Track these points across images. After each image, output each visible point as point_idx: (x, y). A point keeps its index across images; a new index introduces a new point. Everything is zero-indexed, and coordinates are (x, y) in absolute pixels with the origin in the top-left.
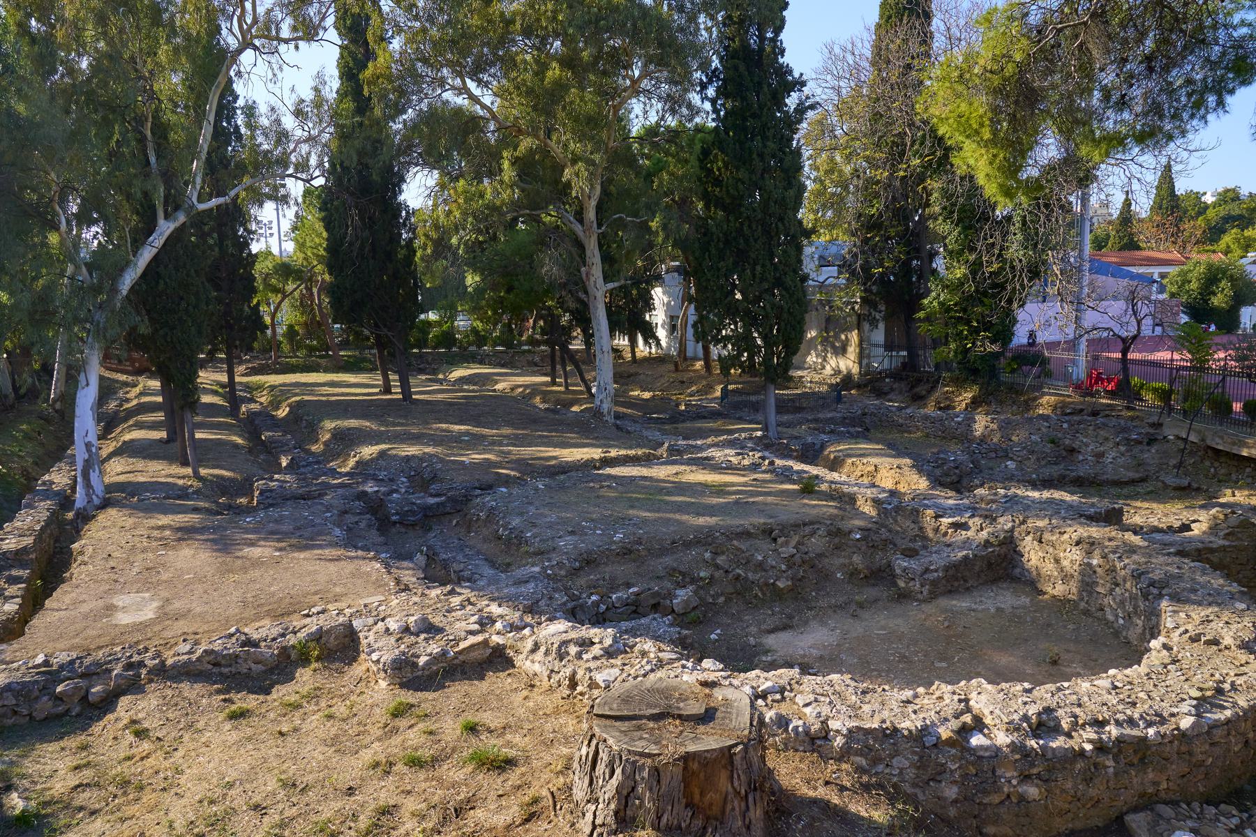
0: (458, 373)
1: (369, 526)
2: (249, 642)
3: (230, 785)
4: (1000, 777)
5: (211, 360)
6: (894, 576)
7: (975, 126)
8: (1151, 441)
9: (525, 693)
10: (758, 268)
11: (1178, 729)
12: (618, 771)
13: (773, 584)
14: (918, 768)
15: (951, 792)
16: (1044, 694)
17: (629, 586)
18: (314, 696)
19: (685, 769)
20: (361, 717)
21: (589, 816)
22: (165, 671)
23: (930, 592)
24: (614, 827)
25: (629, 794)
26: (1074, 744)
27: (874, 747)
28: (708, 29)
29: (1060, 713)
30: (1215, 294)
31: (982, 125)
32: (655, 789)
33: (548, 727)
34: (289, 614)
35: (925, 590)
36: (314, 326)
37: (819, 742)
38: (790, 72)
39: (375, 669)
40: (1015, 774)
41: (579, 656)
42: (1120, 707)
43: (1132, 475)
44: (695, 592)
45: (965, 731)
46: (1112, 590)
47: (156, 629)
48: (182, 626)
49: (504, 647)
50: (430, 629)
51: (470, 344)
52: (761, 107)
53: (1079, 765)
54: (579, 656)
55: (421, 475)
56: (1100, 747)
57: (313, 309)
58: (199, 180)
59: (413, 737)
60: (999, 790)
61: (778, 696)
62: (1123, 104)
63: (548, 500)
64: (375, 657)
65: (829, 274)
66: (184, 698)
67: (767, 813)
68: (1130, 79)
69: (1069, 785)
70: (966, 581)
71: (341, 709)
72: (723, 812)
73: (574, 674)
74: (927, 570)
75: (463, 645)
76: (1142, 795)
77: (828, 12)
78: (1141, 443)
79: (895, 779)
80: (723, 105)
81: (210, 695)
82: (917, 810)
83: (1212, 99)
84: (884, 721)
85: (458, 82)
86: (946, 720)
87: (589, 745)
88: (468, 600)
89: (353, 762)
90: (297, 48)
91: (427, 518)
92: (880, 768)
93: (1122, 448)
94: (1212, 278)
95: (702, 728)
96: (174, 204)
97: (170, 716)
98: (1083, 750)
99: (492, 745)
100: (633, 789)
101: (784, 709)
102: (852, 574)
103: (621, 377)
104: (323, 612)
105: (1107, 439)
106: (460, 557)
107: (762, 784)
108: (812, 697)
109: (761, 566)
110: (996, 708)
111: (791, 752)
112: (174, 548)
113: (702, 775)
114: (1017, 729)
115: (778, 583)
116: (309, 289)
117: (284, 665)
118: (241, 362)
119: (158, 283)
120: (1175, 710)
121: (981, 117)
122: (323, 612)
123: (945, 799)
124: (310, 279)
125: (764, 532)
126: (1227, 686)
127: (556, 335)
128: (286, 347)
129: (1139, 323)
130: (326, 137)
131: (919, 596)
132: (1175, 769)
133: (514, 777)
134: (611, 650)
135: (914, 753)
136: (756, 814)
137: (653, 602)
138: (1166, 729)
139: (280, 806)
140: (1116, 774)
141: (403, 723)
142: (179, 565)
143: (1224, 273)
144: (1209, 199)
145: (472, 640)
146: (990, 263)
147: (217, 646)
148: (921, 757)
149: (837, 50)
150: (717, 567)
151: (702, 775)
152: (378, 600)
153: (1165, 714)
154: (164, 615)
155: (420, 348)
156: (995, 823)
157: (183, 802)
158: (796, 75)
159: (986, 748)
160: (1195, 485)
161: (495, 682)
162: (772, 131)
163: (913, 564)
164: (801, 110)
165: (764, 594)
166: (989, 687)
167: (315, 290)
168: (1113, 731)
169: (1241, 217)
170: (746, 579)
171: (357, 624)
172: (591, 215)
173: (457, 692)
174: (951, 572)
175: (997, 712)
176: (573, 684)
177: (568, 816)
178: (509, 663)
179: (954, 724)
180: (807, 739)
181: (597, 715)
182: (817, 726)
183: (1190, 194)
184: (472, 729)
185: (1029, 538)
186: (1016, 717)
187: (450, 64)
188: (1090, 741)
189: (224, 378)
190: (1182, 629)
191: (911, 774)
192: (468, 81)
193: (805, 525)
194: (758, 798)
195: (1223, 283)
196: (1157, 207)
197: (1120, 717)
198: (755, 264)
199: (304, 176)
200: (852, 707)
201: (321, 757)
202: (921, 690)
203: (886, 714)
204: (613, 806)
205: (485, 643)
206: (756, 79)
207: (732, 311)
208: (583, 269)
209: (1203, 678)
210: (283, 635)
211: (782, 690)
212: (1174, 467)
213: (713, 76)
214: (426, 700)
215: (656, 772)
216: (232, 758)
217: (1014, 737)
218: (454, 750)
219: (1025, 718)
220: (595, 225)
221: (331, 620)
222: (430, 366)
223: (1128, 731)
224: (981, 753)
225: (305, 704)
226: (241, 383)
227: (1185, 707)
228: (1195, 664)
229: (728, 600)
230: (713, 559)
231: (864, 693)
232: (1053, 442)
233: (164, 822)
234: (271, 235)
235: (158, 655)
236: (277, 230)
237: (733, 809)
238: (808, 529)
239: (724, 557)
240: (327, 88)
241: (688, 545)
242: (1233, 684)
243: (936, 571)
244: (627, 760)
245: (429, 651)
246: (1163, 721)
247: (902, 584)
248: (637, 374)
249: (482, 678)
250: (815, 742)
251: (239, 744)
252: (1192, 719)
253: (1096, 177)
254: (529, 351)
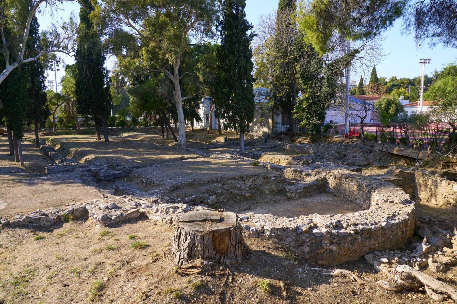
0: (125, 135)
1: (92, 180)
2: (44, 214)
3: (37, 260)
4: (323, 243)
5: (29, 131)
6: (286, 192)
7: (311, 24)
8: (371, 152)
9: (153, 227)
10: (237, 91)
11: (381, 226)
12: (189, 238)
13: (244, 195)
14: (295, 241)
15: (307, 249)
16: (337, 217)
17: (192, 195)
18: (71, 231)
19: (213, 236)
20: (90, 237)
21: (178, 256)
22: (9, 225)
23: (299, 197)
24: (187, 258)
25: (192, 246)
26: (348, 231)
27: (280, 235)
28: (219, 6)
29: (343, 222)
30: (390, 109)
31: (313, 24)
32: (202, 243)
33: (162, 235)
34: (60, 206)
35: (297, 196)
36: (71, 118)
37: (261, 234)
38: (248, 23)
39: (95, 221)
40: (328, 242)
41: (173, 212)
42: (363, 220)
43: (365, 163)
44: (216, 198)
45: (311, 228)
46: (359, 192)
47: (5, 211)
48: (16, 211)
49: (145, 212)
50: (116, 207)
51: (131, 125)
52: (238, 34)
53: (350, 238)
54: (173, 212)
55: (112, 164)
56: (356, 232)
57: (69, 111)
58: (23, 51)
59: (110, 242)
60: (323, 248)
61: (246, 220)
62: (360, 24)
63: (161, 169)
64: (95, 216)
65: (263, 100)
66: (17, 234)
67: (243, 253)
68: (362, 15)
69: (346, 245)
70: (310, 193)
71: (81, 235)
72: (227, 251)
73: (172, 218)
74: (297, 189)
75: (129, 212)
76: (370, 249)
77: (261, 3)
78: (367, 152)
79: (287, 246)
80: (224, 33)
81: (28, 233)
82: (295, 255)
83: (388, 22)
84: (283, 226)
85: (126, 21)
86: (305, 225)
87: (178, 231)
88: (131, 199)
89: (86, 251)
90: (62, 3)
91: (116, 178)
92: (282, 242)
93: (362, 154)
94: (389, 103)
95: (219, 224)
96: (13, 60)
97: (11, 240)
98: (350, 233)
99: (142, 242)
100: (194, 244)
101: (248, 224)
102: (271, 192)
103: (188, 136)
104: (74, 204)
105: (356, 151)
106: (128, 188)
107: (240, 242)
108: (258, 220)
109: (239, 189)
110: (322, 222)
111: (251, 238)
112: (13, 187)
113: (219, 238)
114: (329, 227)
115: (246, 194)
116: (68, 104)
117: (59, 222)
118: (41, 131)
119: (6, 89)
120: (380, 220)
121: (313, 21)
122: (74, 204)
123: (305, 252)
124: (68, 100)
125: (240, 178)
126: (396, 214)
127: (163, 122)
128: (59, 126)
129: (366, 112)
130: (75, 37)
131: (295, 198)
132: (381, 239)
133: (149, 250)
134: (185, 210)
135: (294, 236)
136: (239, 252)
137: (200, 200)
138: (378, 226)
139: (57, 266)
140: (362, 241)
141: (106, 238)
142: (15, 192)
143: (393, 102)
144: (387, 80)
145: (132, 210)
146: (317, 93)
147: (31, 216)
148: (296, 237)
149: (264, 19)
150: (224, 189)
151: (219, 238)
152: (97, 201)
153: (377, 222)
154: (8, 207)
155: (112, 126)
156: (322, 260)
157: (17, 267)
158: (250, 23)
159: (318, 233)
160: (385, 166)
161: (141, 224)
162: (242, 43)
163: (293, 187)
164: (252, 36)
165: (241, 198)
166: (319, 215)
167: (70, 105)
168: (360, 227)
169: (397, 85)
170: (234, 193)
171: (88, 207)
172: (176, 72)
173: (127, 228)
174: (305, 190)
175: (322, 222)
176: (171, 222)
177: (170, 258)
178: (147, 218)
179: (308, 226)
180: (257, 233)
181: (181, 222)
182: (260, 229)
183: (381, 78)
184: (133, 238)
185: (331, 178)
186: (328, 223)
187: (124, 14)
188: (353, 230)
189: (34, 137)
190: (382, 199)
191: (293, 243)
192: (130, 20)
193: (255, 175)
194: (239, 246)
195: (392, 105)
196: (371, 81)
197: (363, 223)
198: (236, 90)
199: (66, 52)
200: (273, 222)
201: (74, 250)
202: (296, 218)
203: (284, 224)
204: (187, 251)
205: (138, 211)
206: (236, 24)
207: (229, 107)
208: (174, 92)
209: (389, 212)
210: (58, 212)
211: (248, 218)
212: (378, 160)
213: (220, 23)
214: (116, 230)
215: (203, 237)
216: (37, 252)
217: (328, 229)
218: (126, 245)
219: (331, 224)
220: (178, 76)
221: (78, 205)
222: (116, 133)
223: (365, 226)
224: (317, 235)
225: (67, 234)
226: (41, 138)
227: (383, 219)
228: (386, 208)
229: (228, 200)
230: (222, 186)
231: (276, 218)
232: (339, 153)
233: (9, 273)
234: (53, 85)
235: (6, 219)
236: (56, 79)
237: (231, 250)
238: (256, 177)
239: (226, 186)
240: (75, 18)
241: (213, 182)
242: (398, 213)
243: (300, 189)
244: (192, 234)
245: (116, 214)
246: (376, 224)
247: (289, 195)
248: (194, 135)
249: (136, 222)
250: (260, 234)
251: (40, 248)
252: (386, 223)
253: (352, 64)
254: (154, 128)
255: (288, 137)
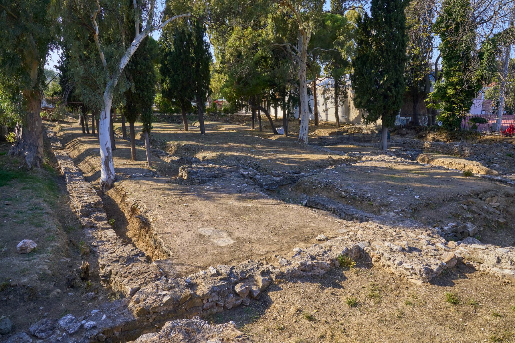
125: (475, 194)
155: (177, 113)
230: (468, 208)
255: (412, 131)
